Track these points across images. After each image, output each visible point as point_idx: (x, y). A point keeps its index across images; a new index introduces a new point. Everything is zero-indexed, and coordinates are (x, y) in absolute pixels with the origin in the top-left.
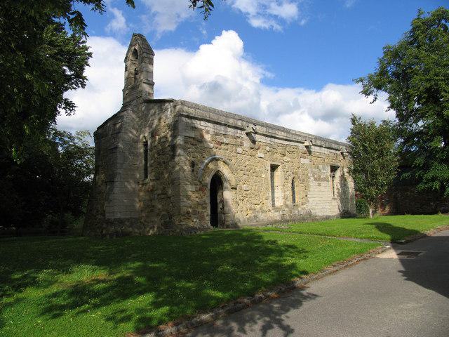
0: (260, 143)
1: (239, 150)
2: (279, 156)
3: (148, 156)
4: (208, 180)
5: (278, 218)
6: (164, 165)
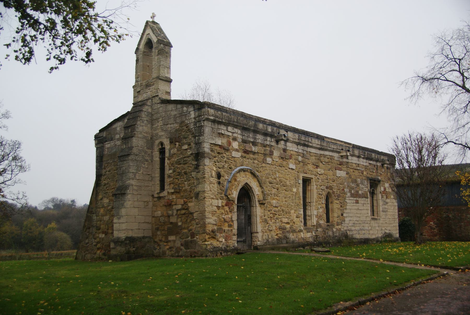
0: (292, 152)
1: (269, 160)
2: (310, 167)
3: (166, 164)
4: (235, 194)
5: (311, 240)
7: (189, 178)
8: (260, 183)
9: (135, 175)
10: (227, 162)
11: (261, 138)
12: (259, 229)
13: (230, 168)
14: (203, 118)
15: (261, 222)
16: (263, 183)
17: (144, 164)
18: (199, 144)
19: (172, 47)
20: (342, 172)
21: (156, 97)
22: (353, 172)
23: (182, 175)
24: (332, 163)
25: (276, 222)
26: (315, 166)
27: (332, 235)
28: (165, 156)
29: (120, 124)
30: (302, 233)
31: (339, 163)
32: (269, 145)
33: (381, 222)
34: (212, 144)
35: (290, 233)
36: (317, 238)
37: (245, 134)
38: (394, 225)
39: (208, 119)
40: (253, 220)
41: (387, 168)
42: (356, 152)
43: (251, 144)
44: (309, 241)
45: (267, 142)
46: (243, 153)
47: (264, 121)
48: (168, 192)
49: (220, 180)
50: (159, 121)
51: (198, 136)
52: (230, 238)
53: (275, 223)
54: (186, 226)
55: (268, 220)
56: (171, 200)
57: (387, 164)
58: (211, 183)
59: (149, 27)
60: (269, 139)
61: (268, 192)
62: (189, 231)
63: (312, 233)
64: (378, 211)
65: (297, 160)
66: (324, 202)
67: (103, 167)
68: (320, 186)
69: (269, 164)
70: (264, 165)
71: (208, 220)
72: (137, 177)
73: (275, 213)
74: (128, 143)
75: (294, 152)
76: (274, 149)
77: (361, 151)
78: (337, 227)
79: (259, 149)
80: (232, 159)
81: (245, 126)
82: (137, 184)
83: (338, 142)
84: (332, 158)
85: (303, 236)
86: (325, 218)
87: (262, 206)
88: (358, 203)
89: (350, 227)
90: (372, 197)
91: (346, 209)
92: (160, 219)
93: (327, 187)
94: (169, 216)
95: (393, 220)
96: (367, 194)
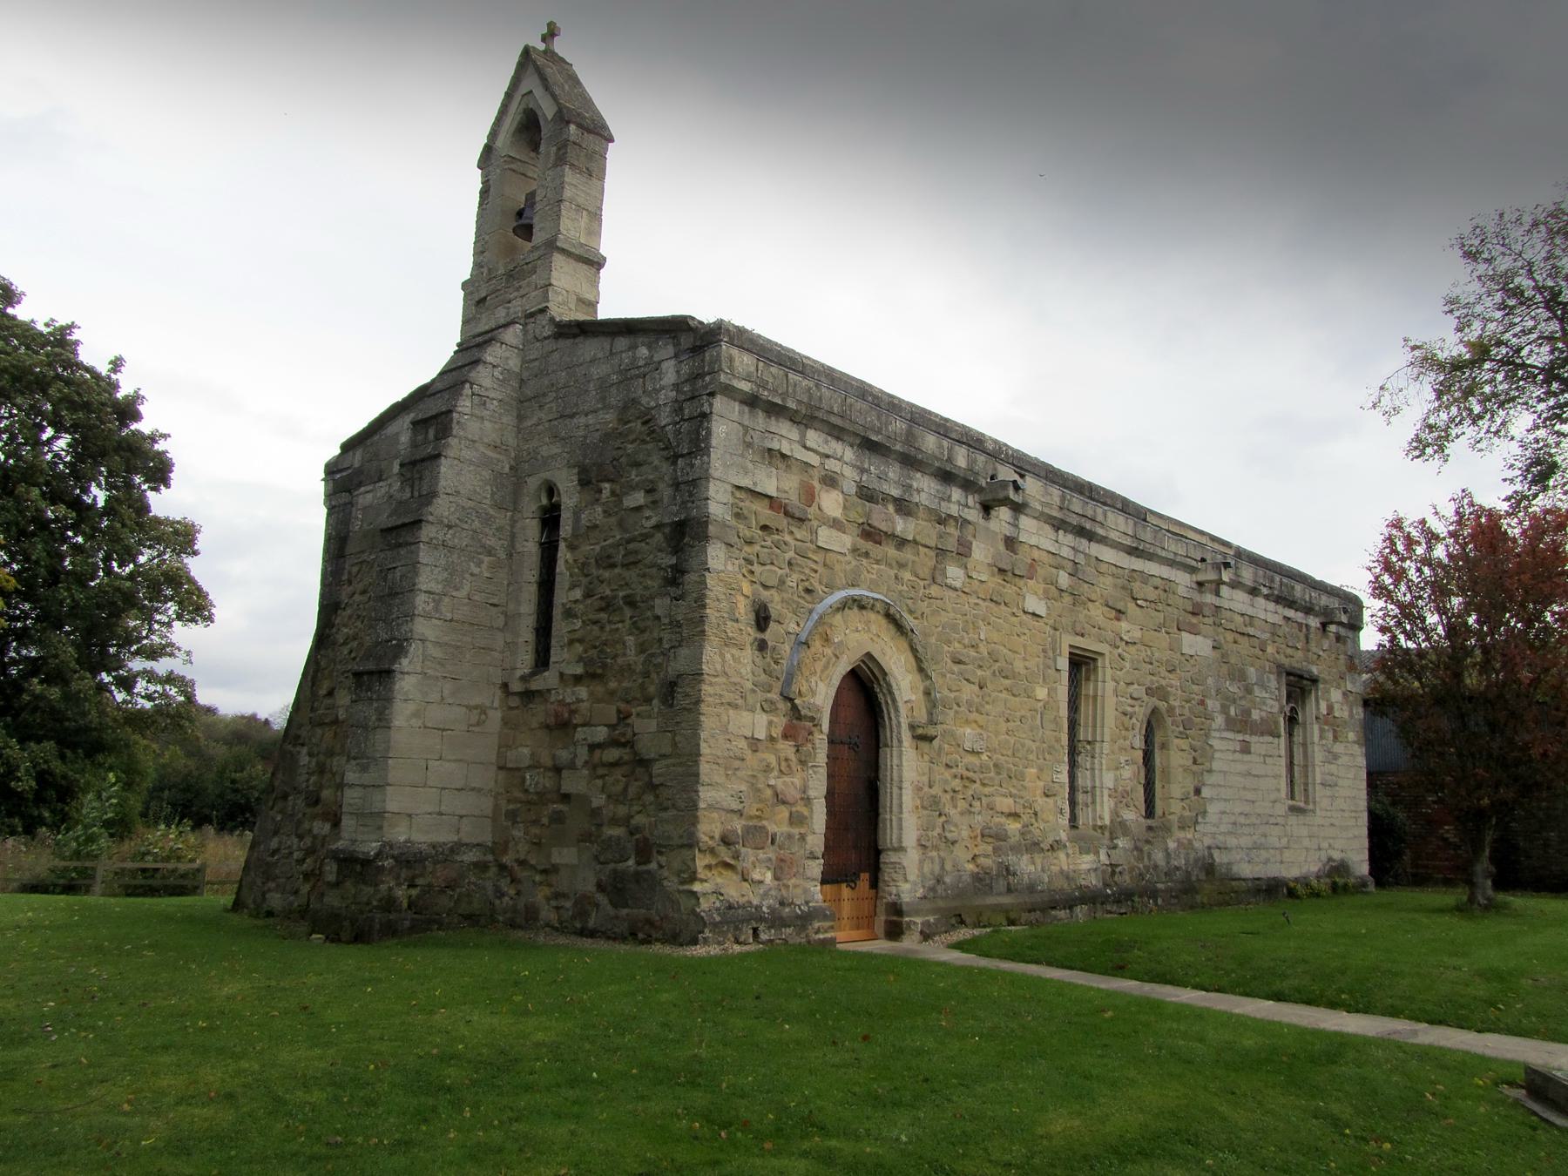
0: (1036, 554)
1: (954, 574)
2: (1097, 612)
3: (561, 567)
4: (821, 693)
5: (1093, 881)
6: (628, 612)
7: (643, 620)
8: (918, 660)
9: (437, 603)
10: (797, 564)
11: (929, 486)
12: (910, 837)
13: (808, 591)
14: (710, 383)
15: (917, 807)
16: (929, 656)
17: (479, 564)
18: (691, 487)
19: (612, 140)
20: (1199, 638)
21: (540, 317)
22: (1235, 642)
23: (620, 609)
24: (1169, 605)
25: (973, 810)
26: (1114, 612)
27: (1164, 864)
28: (559, 536)
29: (406, 421)
30: (1062, 855)
31: (1190, 609)
32: (955, 519)
33: (1318, 821)
34: (738, 488)
35: (1022, 855)
36: (1113, 873)
37: (870, 465)
38: (1356, 833)
39: (729, 391)
40: (884, 800)
41: (1338, 638)
42: (1247, 574)
43: (891, 508)
44: (1087, 887)
45: (952, 505)
46: (858, 539)
47: (943, 427)
48: (562, 675)
49: (767, 636)
50: (546, 403)
51: (689, 454)
52: (795, 870)
53: (970, 812)
54: (622, 810)
55: (943, 800)
56: (569, 704)
57: (1340, 624)
58: (728, 642)
59: (531, 69)
60: (956, 494)
61: (946, 692)
62: (632, 834)
63: (1097, 853)
64: (1306, 784)
65: (1054, 583)
66: (1139, 742)
67: (345, 577)
68: (1128, 684)
69: (956, 589)
70: (934, 590)
71: (709, 794)
72: (444, 609)
73: (971, 774)
74: (421, 478)
75: (1045, 554)
76: (974, 537)
77: (1261, 573)
78: (1181, 835)
79: (920, 527)
80: (815, 558)
81: (874, 438)
82: (446, 639)
83: (1191, 535)
84: (1167, 587)
85: (1065, 868)
86: (1143, 799)
87: (924, 745)
88: (1250, 753)
89: (1221, 838)
90: (1291, 734)
91: (1210, 771)
92: (524, 780)
93: (1150, 688)
94: (558, 770)
95: (1353, 814)
96: (1276, 723)
